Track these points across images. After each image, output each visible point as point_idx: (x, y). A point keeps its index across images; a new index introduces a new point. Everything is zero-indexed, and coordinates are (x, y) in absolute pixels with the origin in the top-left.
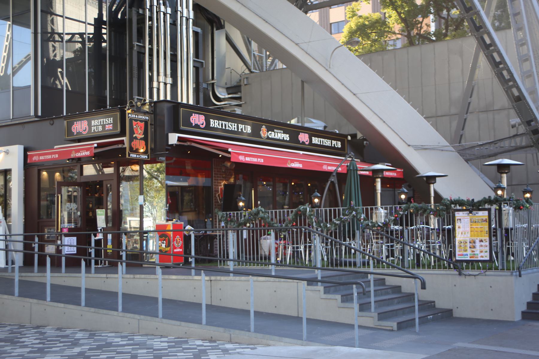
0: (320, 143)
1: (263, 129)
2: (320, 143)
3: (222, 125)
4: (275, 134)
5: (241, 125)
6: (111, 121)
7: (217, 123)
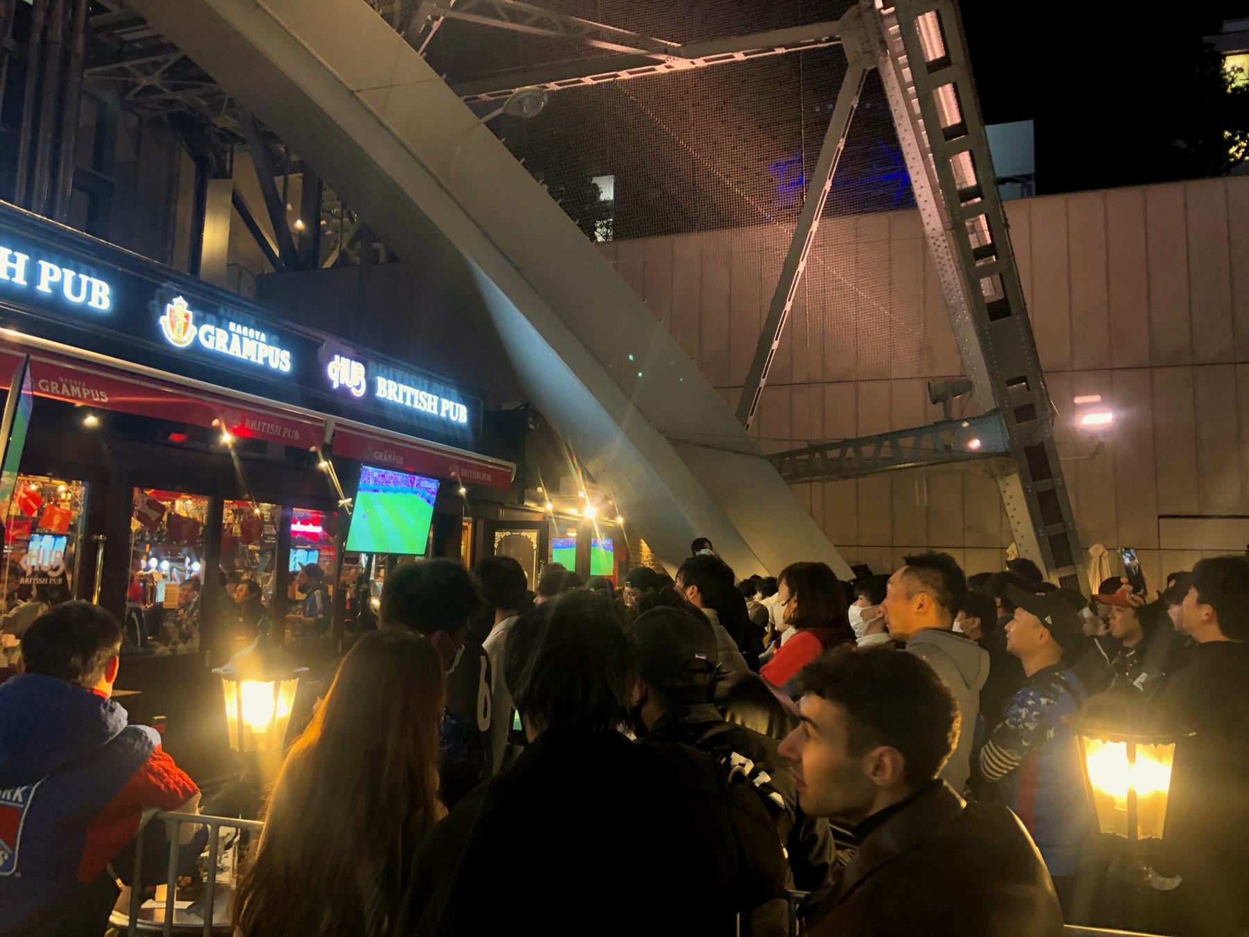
0: (405, 399)
1: (172, 311)
2: (405, 399)
3: (405, 394)
4: (230, 338)
5: (56, 268)
6: (277, 433)
7: (433, 401)
